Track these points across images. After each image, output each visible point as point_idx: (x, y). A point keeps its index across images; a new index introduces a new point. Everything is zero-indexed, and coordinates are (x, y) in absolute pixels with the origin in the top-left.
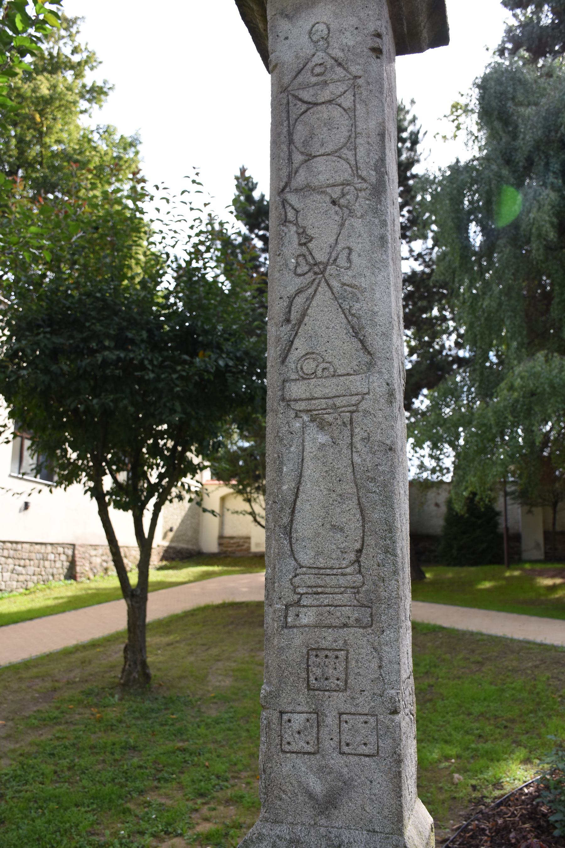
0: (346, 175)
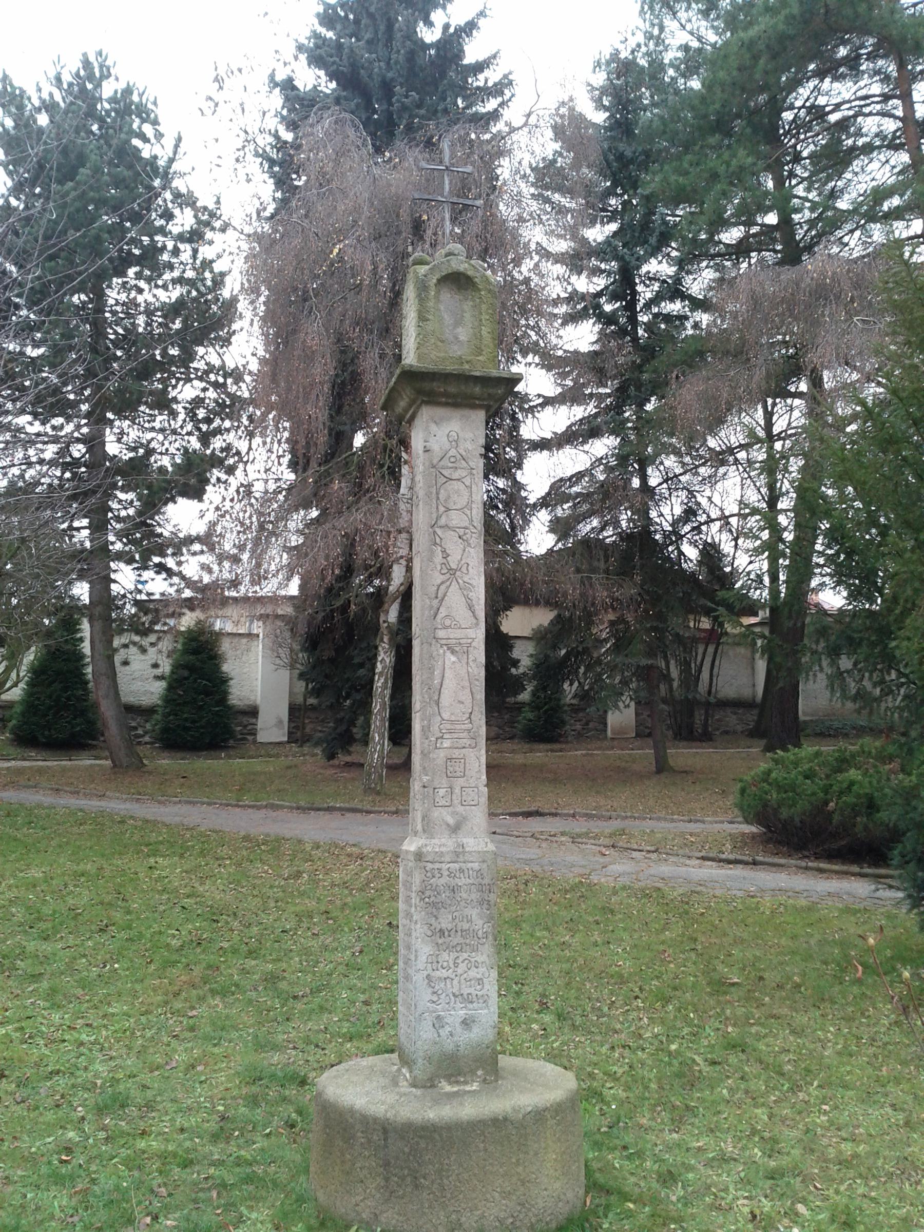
0: (466, 524)
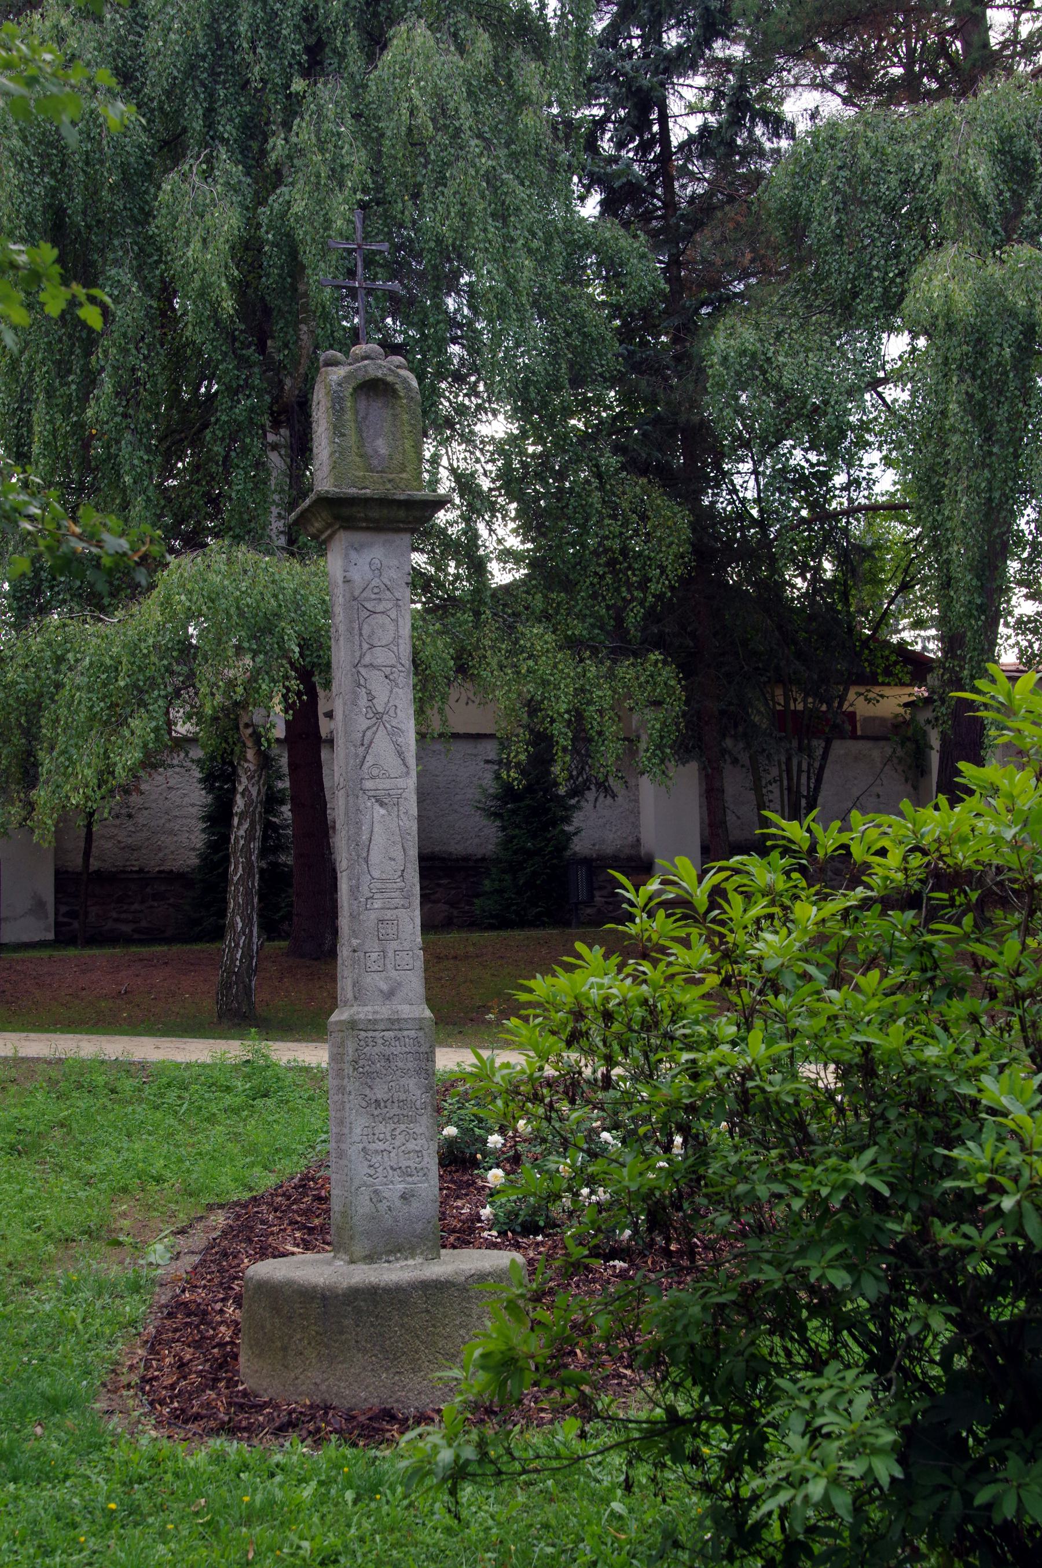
0: (393, 662)
